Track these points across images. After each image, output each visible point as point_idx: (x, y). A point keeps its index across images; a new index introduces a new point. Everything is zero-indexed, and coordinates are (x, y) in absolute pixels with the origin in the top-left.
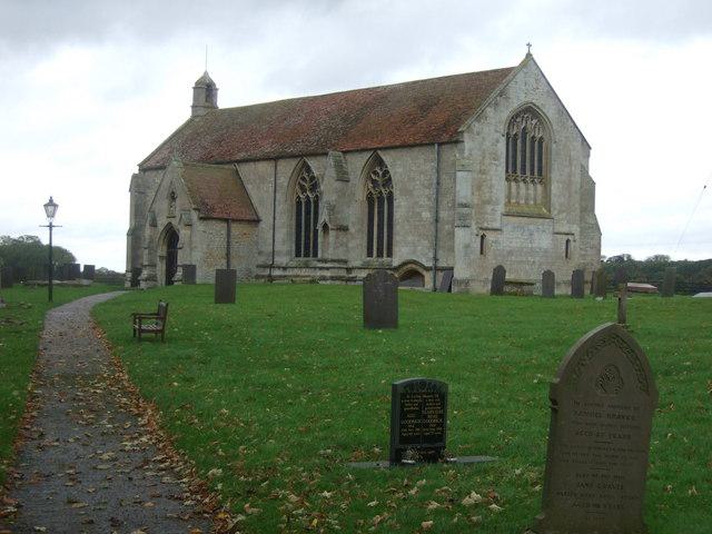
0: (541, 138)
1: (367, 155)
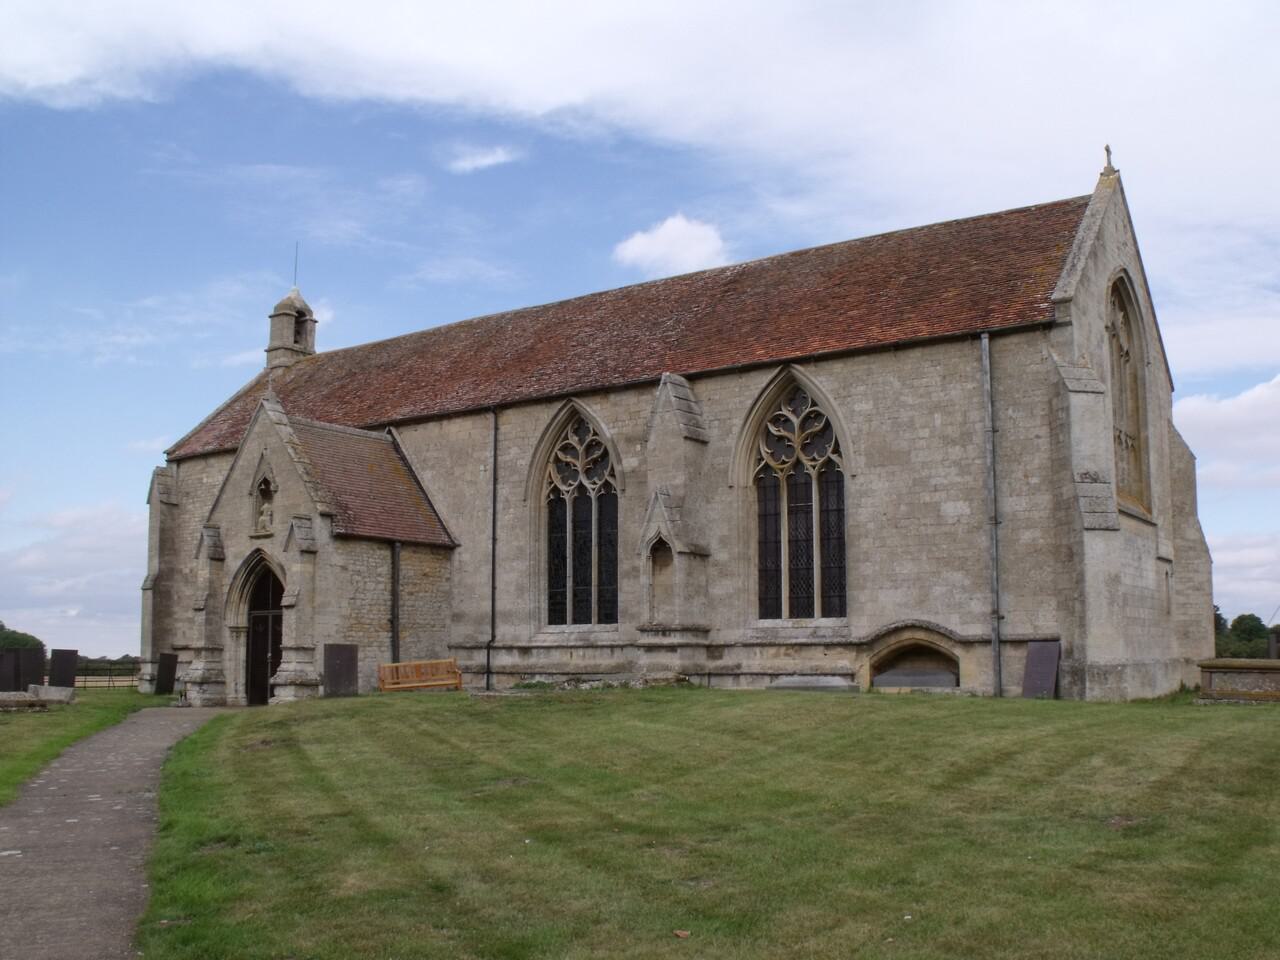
1: (762, 379)
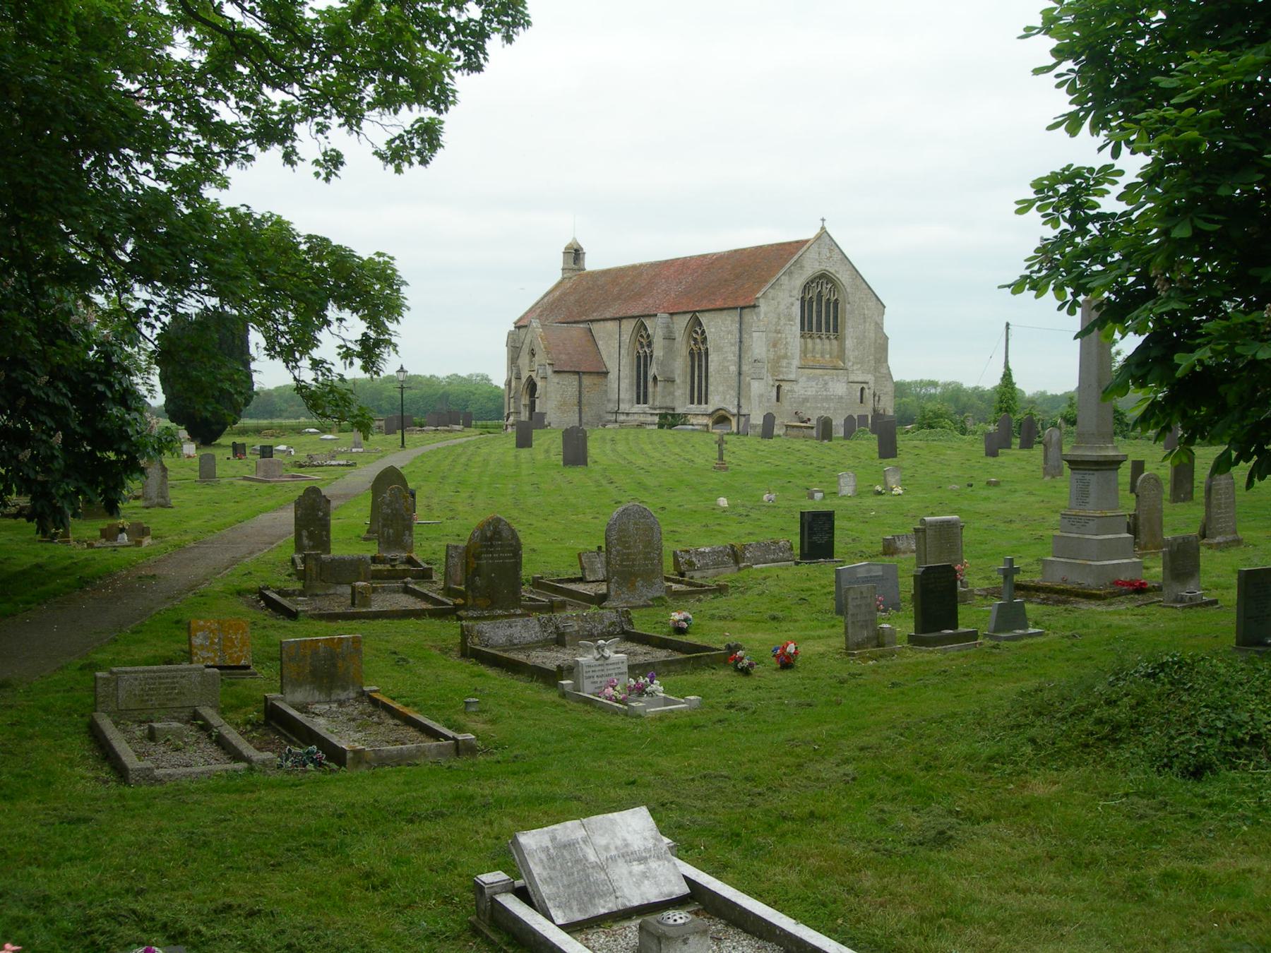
0: (836, 300)
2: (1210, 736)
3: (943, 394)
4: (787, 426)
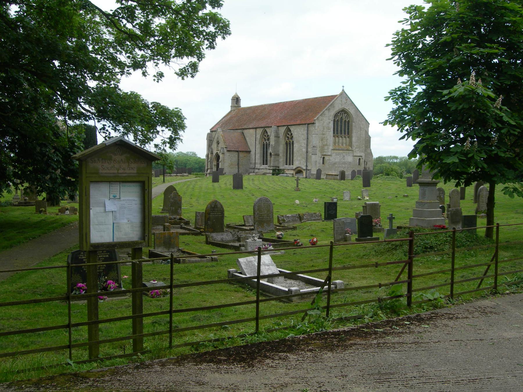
1: (285, 127)
2: (420, 247)
3: (400, 162)
4: (327, 175)
